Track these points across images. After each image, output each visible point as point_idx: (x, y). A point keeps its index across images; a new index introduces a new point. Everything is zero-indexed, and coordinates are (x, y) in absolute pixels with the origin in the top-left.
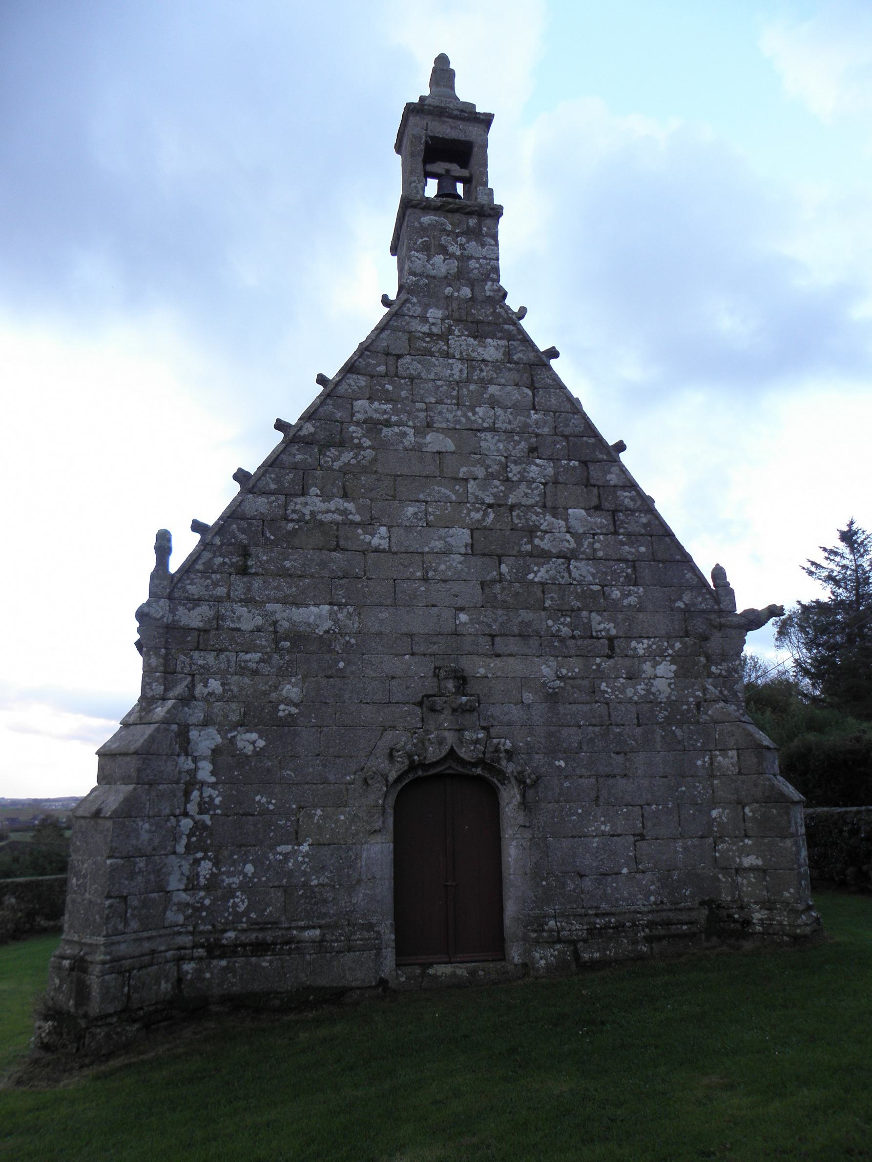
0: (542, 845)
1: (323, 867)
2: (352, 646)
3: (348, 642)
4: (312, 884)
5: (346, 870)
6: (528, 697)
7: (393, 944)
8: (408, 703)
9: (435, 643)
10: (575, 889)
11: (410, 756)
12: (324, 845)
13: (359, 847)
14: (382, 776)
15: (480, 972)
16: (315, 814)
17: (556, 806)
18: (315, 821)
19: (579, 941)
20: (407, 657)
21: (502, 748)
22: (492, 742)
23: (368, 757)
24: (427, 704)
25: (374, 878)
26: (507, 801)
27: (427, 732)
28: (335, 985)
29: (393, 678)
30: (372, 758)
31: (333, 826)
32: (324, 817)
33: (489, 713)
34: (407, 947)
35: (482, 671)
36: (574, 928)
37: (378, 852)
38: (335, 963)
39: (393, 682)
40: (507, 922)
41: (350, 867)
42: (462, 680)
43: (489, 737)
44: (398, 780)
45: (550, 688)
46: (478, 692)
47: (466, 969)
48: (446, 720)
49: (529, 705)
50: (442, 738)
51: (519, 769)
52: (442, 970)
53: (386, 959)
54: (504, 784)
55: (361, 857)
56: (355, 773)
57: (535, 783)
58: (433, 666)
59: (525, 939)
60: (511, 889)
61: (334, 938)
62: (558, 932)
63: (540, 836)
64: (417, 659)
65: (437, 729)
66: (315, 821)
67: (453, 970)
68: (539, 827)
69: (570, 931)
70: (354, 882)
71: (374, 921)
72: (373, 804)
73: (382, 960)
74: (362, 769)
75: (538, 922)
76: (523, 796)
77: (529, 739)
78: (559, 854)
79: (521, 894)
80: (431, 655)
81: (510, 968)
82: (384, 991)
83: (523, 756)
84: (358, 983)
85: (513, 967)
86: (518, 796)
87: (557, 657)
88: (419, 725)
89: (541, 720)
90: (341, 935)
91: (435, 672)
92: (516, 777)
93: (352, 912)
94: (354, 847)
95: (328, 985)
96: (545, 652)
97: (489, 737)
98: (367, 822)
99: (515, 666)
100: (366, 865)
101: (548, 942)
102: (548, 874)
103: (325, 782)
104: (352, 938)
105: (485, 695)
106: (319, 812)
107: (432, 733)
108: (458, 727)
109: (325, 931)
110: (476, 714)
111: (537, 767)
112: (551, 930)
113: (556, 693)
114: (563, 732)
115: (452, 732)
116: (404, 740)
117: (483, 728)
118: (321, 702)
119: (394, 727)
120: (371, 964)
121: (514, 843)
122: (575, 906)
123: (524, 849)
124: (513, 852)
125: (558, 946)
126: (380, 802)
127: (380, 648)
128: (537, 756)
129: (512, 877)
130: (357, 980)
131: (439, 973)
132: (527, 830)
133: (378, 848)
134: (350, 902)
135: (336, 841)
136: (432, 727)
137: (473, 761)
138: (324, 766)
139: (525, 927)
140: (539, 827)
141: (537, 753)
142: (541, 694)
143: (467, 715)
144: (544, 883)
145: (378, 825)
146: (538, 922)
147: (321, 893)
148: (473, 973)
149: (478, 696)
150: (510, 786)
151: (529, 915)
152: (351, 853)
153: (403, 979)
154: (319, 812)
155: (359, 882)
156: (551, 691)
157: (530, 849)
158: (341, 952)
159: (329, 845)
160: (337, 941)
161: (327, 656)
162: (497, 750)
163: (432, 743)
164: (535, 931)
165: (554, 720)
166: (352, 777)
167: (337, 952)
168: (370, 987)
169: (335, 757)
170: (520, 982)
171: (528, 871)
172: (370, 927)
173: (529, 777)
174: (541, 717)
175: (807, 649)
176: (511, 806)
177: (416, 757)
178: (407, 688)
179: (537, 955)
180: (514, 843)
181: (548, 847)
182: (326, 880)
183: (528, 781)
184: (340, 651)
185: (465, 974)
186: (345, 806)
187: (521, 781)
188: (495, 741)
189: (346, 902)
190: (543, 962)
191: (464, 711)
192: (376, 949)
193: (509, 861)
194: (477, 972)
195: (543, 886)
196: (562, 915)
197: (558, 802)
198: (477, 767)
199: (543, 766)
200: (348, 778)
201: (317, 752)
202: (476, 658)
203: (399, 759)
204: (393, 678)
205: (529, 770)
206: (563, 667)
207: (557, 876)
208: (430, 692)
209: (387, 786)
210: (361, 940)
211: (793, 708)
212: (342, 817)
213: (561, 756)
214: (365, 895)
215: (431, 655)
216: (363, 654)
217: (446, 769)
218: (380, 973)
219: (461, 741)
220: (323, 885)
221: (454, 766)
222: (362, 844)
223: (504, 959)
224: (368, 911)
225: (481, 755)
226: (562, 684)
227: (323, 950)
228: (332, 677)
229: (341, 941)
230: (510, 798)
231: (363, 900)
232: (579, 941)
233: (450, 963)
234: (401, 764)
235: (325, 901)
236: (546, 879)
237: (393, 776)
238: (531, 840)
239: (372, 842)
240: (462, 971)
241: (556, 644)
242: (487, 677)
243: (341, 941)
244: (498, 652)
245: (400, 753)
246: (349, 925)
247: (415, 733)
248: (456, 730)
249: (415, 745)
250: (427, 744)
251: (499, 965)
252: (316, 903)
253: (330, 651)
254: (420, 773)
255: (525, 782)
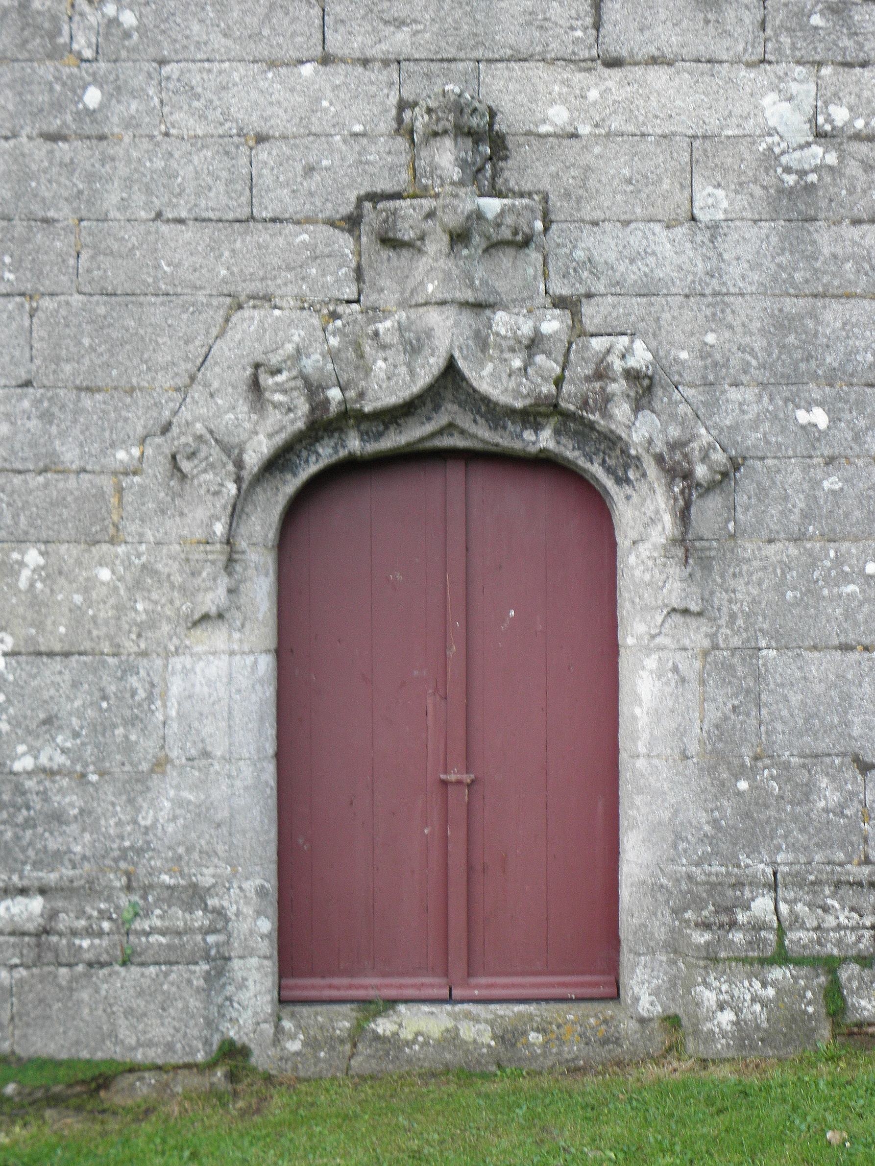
0: (740, 671)
1: (48, 721)
2: (127, 35)
3: (114, 22)
4: (18, 766)
5: (120, 731)
6: (713, 200)
7: (267, 947)
8: (309, 220)
9: (400, 23)
10: (842, 806)
11: (313, 389)
12: (51, 654)
13: (159, 662)
14: (226, 449)
15: (534, 1037)
16: (22, 564)
17: (793, 550)
18: (23, 584)
19: (845, 960)
20: (307, 70)
21: (618, 365)
22: (586, 348)
23: (183, 390)
24: (374, 224)
25: (206, 754)
26: (633, 535)
27: (375, 312)
28: (85, 1054)
29: (261, 139)
30: (197, 392)
31: (78, 599)
32: (50, 574)
33: (579, 254)
34: (300, 958)
35: (559, 115)
36: (830, 921)
37: (219, 684)
38: (85, 995)
39: (263, 154)
40: (625, 894)
41: (131, 722)
42: (487, 143)
43: (578, 330)
44: (278, 462)
45: (788, 170)
46: (545, 184)
47: (491, 1023)
48: (432, 271)
49: (714, 228)
50: (411, 335)
51: (674, 432)
52: (419, 1024)
53: (242, 986)
54: (628, 481)
55: (164, 696)
56: (143, 441)
57: (726, 477)
58: (393, 100)
59: (675, 947)
60: (638, 800)
61: (83, 923)
62: (781, 932)
63: (736, 641)
64: (339, 74)
65: (405, 304)
66: (23, 584)
67: (450, 1024)
68: (733, 617)
69: (818, 928)
70: (145, 767)
71: (206, 879)
72: (199, 534)
73: (230, 989)
74: (166, 429)
75: (720, 904)
76: (684, 516)
77: (711, 338)
78: (795, 699)
79: (666, 815)
80: (386, 63)
81: (629, 1026)
82: (232, 1077)
83: (689, 392)
84: (154, 1055)
85: (633, 1025)
86: (667, 519)
87: (820, 64)
88: (350, 291)
89: (755, 276)
90: (104, 915)
91: (399, 120)
92: (659, 459)
93: (140, 852)
94: (144, 662)
95: (64, 1056)
96: (779, 50)
97: (578, 330)
98: (183, 589)
99: (671, 99)
100: (181, 716)
101: (745, 961)
102: (756, 758)
103: (50, 466)
104: (137, 925)
105: (567, 195)
106: (33, 557)
107: (387, 314)
108: (469, 296)
109: (60, 904)
110: (534, 255)
111: (735, 428)
112: (758, 926)
113: (810, 188)
114: (828, 316)
115: (451, 312)
116: (292, 335)
117: (560, 303)
118: (31, 218)
119: (267, 298)
120: (194, 1003)
121: (651, 662)
122: (840, 856)
123: (683, 680)
124: (653, 692)
125: (777, 973)
126: (219, 528)
127: (218, 41)
128: (734, 394)
129: (641, 763)
130: (150, 1044)
131: (407, 1034)
132: (693, 622)
133: (217, 667)
134: (135, 822)
135: (87, 645)
136: (389, 297)
137: (519, 404)
138: (47, 417)
139: (677, 912)
140: (733, 617)
141: (736, 384)
142: (758, 191)
143: (505, 259)
144: (743, 785)
145: (213, 599)
146: (720, 904)
147: (44, 796)
148: (509, 1037)
149: (546, 199)
150: (644, 487)
151: (690, 877)
152: (133, 681)
153: (294, 1046)
154: (33, 557)
155: (160, 764)
156: (791, 179)
157: (703, 682)
158: (102, 965)
159: (67, 655)
160: (89, 932)
161: (46, 70)
162: (601, 374)
163: (384, 347)
164: (706, 926)
165: (798, 276)
166: (136, 452)
167: (90, 965)
168: (188, 1066)
169: (79, 389)
170: (652, 1071)
171: (693, 748)
172: (194, 896)
173: (705, 458)
174: (755, 266)
175: (386, 319)
176: (644, 549)
177: (334, 394)
178: (310, 170)
179: (709, 997)
180: (651, 662)
181: (758, 677)
182: (61, 759)
183: (701, 471)
184: (88, 54)
185: (487, 1038)
186: (112, 541)
187: (677, 472)
188: (597, 344)
189: (120, 823)
190: (726, 1018)
191: (494, 246)
192: (207, 958)
193: (634, 718)
194: (525, 1033)
195: (740, 794)
196: (798, 881)
197: (798, 539)
198: (537, 428)
199: (755, 425)
200: (121, 455)
201: (24, 376)
202: (538, 72)
203: (278, 397)
204: (261, 139)
205: (704, 437)
206: (836, 97)
207: (786, 766)
208: (384, 185)
209: (238, 480)
210: (163, 934)
211: (373, 1025)
212: (105, 574)
213: (816, 395)
214: (179, 803)
215: (386, 63)
216: (162, 62)
217: (440, 432)
218: (225, 1026)
219: (481, 341)
220: (51, 773)
221: (465, 421)
222: (168, 655)
223: (616, 997)
224: (189, 850)
225: (548, 388)
226: (832, 159)
227: (49, 956)
228: (65, 138)
229: (101, 934)
230: (643, 518)
231: (174, 818)
232: (845, 960)
233: (450, 1000)
234: (287, 417)
235: (58, 818)
236: (750, 773)
237: (259, 450)
238: (706, 653)
239: (199, 649)
240: (475, 1027)
241: (816, 20)
242: (574, 136)
243: (101, 934)
244: (616, 50)
245: (280, 378)
246: (129, 888)
247: (334, 316)
248: (465, 305)
249: (333, 355)
250: (368, 348)
251: (592, 1015)
252: (29, 824)
253: (55, 53)
254: (354, 444)
255: (687, 475)
